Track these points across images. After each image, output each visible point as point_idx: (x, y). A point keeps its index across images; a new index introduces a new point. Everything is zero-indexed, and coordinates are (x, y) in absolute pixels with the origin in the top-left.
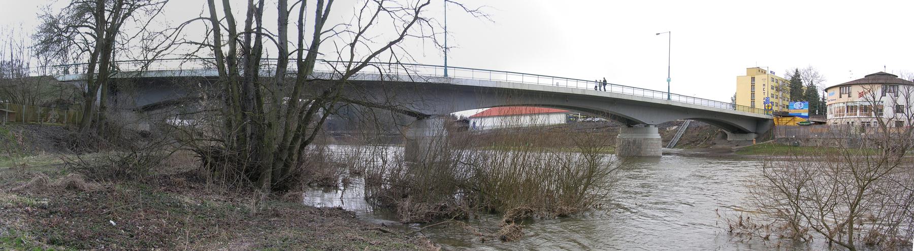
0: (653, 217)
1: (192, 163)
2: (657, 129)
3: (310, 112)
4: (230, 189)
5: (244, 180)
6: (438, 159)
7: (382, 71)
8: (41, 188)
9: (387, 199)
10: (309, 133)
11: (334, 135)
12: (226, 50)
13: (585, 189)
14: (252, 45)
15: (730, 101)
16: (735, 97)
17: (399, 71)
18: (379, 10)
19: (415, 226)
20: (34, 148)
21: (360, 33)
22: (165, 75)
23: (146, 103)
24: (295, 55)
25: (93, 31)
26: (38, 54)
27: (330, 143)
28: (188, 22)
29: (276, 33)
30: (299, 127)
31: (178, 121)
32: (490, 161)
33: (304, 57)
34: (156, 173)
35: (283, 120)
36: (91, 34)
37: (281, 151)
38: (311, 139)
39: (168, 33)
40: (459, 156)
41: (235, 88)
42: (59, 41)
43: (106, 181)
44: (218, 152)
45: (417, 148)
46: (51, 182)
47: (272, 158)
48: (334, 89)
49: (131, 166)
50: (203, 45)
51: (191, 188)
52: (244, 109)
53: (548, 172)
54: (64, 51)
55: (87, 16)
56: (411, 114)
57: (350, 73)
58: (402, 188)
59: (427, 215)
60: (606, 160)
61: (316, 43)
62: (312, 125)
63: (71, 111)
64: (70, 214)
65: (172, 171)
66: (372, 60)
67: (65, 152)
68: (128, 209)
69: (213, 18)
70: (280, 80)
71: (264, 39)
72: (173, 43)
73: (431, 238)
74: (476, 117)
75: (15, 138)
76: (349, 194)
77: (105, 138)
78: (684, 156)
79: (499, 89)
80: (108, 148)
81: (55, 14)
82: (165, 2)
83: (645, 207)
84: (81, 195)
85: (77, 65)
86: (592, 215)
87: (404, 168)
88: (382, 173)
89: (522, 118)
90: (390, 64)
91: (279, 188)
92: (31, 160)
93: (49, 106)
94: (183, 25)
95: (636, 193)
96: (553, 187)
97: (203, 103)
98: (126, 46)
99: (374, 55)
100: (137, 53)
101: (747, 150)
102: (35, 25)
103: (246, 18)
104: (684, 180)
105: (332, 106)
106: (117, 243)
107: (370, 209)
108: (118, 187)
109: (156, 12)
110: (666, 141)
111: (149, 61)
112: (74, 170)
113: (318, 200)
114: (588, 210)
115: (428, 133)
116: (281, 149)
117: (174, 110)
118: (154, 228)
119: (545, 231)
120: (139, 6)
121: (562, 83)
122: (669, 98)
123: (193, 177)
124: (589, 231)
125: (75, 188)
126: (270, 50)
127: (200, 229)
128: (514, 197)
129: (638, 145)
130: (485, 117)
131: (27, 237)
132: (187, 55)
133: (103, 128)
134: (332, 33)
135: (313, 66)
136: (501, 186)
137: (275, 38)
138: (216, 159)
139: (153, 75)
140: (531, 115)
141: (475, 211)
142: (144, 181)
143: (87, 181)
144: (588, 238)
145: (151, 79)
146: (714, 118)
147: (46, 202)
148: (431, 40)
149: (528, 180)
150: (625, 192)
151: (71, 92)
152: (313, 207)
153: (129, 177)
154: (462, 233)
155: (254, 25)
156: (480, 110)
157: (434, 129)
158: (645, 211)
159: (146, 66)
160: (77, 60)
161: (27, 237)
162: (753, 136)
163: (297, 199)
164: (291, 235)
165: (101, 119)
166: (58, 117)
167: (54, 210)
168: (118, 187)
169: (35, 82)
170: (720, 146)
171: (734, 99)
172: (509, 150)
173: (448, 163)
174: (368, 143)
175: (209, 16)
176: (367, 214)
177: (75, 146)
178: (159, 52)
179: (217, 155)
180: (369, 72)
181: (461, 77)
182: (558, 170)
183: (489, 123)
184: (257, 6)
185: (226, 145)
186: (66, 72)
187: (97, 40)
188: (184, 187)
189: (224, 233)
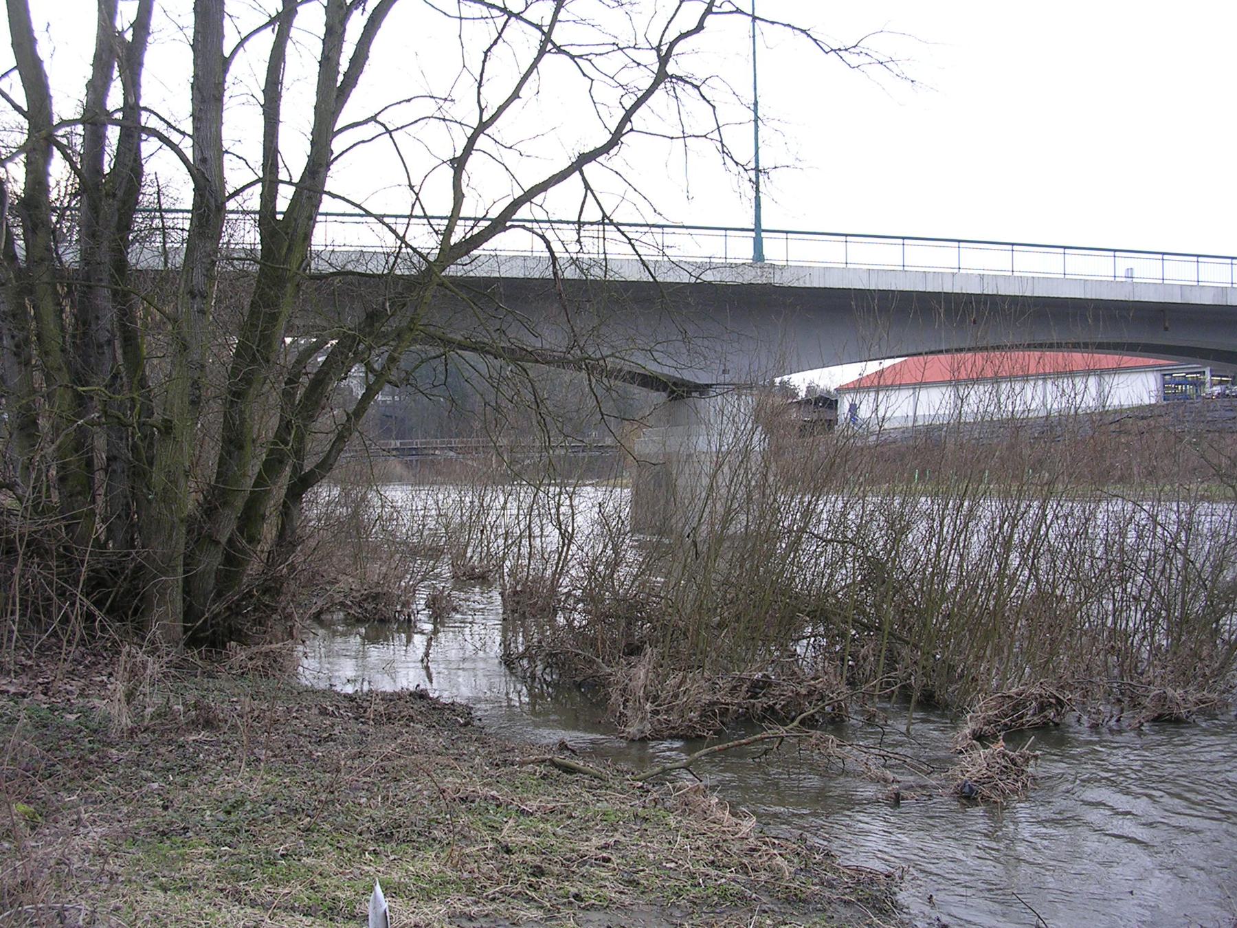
3: (320, 381)
5: (90, 617)
6: (739, 524)
7: (557, 247)
9: (578, 662)
10: (317, 447)
17: (611, 248)
18: (542, 52)
19: (669, 751)
21: (482, 127)
24: (252, 198)
27: (388, 479)
30: (285, 426)
33: (282, 204)
38: (325, 466)
40: (808, 513)
45: (672, 488)
48: (399, 304)
56: (650, 381)
57: (450, 252)
58: (624, 624)
59: (708, 712)
61: (320, 162)
62: (327, 421)
66: (523, 212)
70: (198, 279)
71: (149, 146)
73: (722, 787)
74: (857, 387)
76: (449, 645)
79: (948, 296)
87: (630, 556)
88: (559, 573)
90: (580, 224)
91: (209, 637)
99: (528, 196)
103: (89, 73)
105: (392, 360)
107: (520, 696)
113: (347, 669)
115: (704, 443)
126: (167, 176)
130: (887, 388)
134: (372, 129)
135: (308, 236)
148: (710, 148)
152: (330, 693)
154: (826, 773)
155: (115, 99)
156: (873, 367)
157: (721, 430)
163: (276, 665)
164: (255, 790)
173: (772, 537)
174: (512, 476)
176: (511, 713)
180: (513, 250)
181: (805, 259)
184: (129, 36)
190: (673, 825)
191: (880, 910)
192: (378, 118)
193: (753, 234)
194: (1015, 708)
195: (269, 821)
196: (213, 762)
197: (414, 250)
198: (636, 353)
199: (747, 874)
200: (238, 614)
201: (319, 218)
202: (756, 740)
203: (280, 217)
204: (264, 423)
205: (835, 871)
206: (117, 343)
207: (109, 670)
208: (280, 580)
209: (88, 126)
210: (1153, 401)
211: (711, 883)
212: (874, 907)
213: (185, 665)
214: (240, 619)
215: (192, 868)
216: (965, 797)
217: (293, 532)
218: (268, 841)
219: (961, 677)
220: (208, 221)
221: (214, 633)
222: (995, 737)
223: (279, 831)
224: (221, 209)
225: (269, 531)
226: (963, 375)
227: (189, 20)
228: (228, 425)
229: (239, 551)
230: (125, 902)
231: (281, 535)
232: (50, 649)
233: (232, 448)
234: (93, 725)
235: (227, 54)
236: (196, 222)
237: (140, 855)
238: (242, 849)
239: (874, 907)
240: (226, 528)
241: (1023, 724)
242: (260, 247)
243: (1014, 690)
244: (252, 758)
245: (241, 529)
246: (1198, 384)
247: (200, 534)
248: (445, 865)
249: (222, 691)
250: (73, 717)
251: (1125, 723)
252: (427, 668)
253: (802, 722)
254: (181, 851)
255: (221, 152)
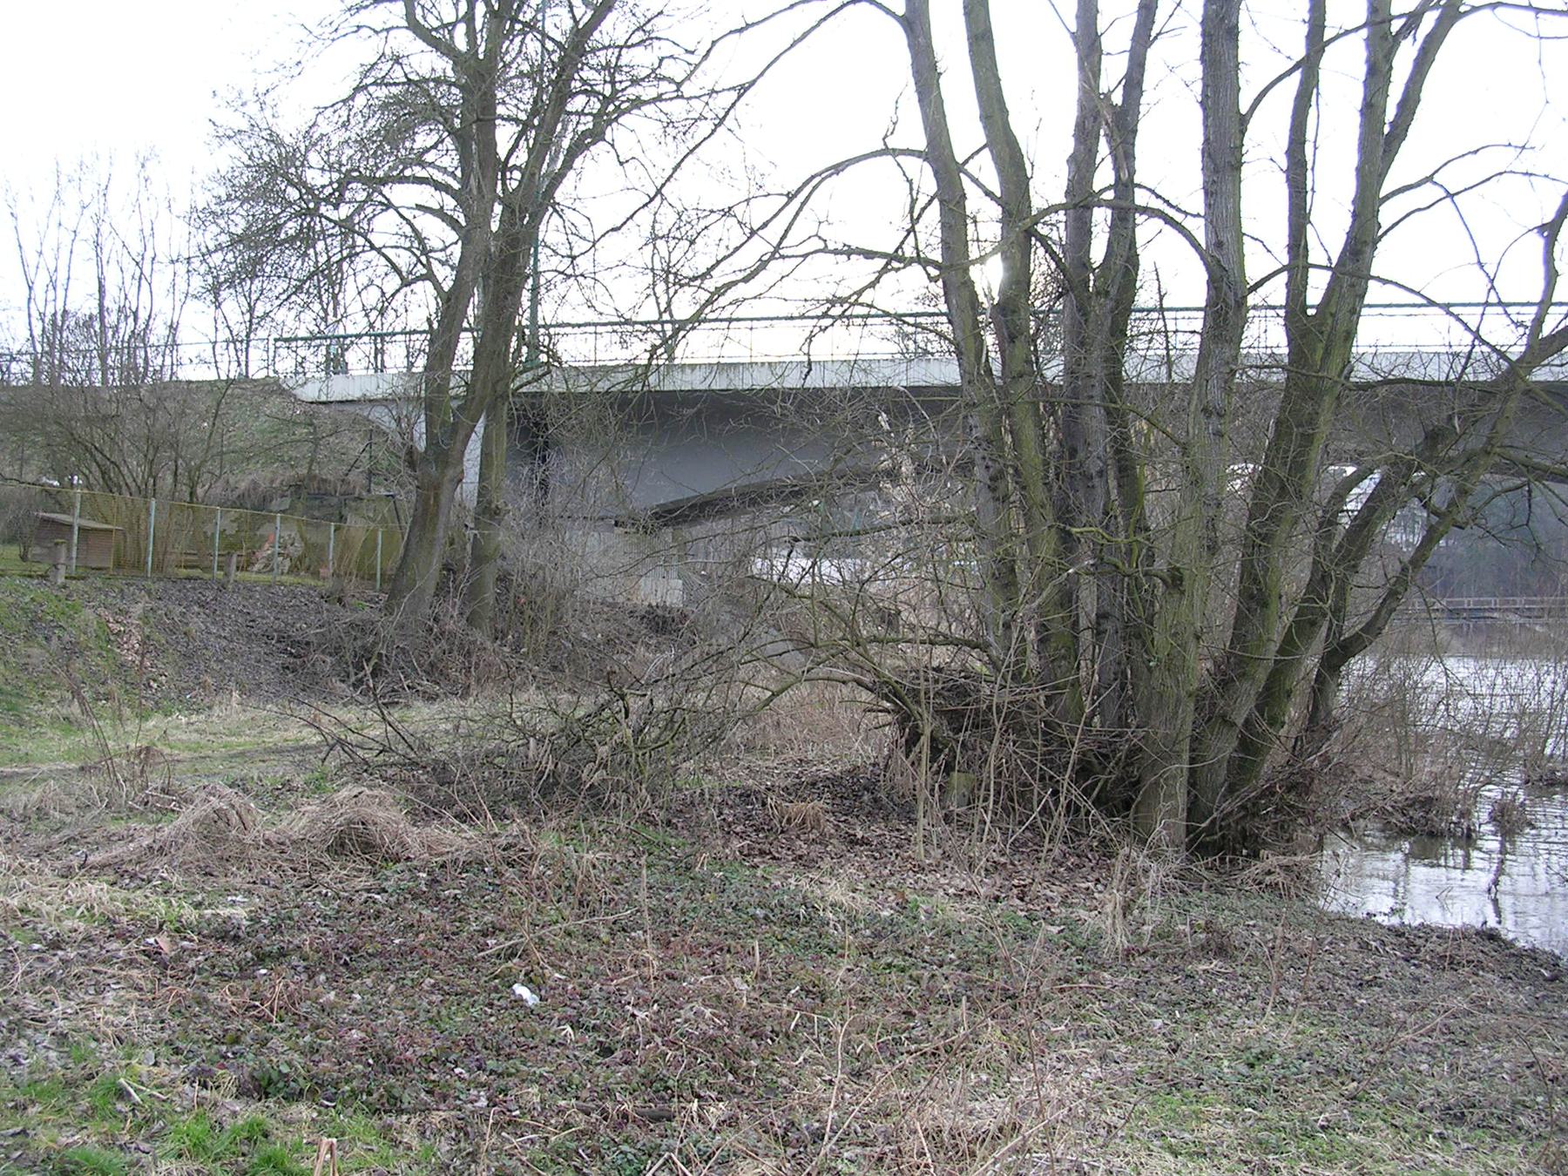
1: (856, 737)
4: (1017, 847)
5: (1073, 809)
8: (218, 848)
10: (1361, 605)
11: (1453, 613)
12: (989, 278)
14: (1098, 253)
20: (195, 679)
22: (743, 382)
23: (667, 494)
24: (1276, 292)
25: (450, 203)
26: (215, 290)
28: (837, 169)
29: (1195, 202)
30: (1320, 580)
31: (798, 565)
33: (1314, 296)
34: (709, 782)
35: (1231, 560)
36: (440, 213)
37: (1225, 684)
38: (1373, 628)
39: (756, 218)
41: (1029, 432)
42: (306, 238)
43: (502, 817)
44: (961, 692)
46: (264, 824)
47: (1188, 713)
48: (1471, 421)
49: (603, 751)
50: (895, 260)
51: (853, 841)
52: (1065, 514)
54: (328, 278)
55: (423, 139)
61: (1364, 237)
62: (1372, 573)
63: (356, 525)
64: (344, 961)
65: (769, 770)
67: (328, 696)
68: (590, 937)
69: (938, 153)
70: (1215, 395)
71: (1145, 229)
72: (776, 253)
75: (110, 638)
77: (499, 635)
80: (510, 680)
81: (290, 127)
82: (743, 89)
84: (394, 877)
85: (380, 338)
91: (1221, 843)
92: (176, 731)
93: (265, 501)
94: (814, 181)
97: (899, 494)
98: (584, 264)
100: (628, 293)
102: (197, 168)
103: (1068, 146)
106: (541, 1081)
108: (548, 843)
109: (705, 128)
111: (681, 326)
112: (362, 770)
116: (1227, 675)
117: (781, 521)
118: (698, 1016)
120: (637, 103)
123: (859, 796)
125: (368, 846)
126: (1172, 275)
127: (891, 1018)
131: (146, 1070)
132: (834, 301)
133: (489, 596)
134: (1429, 193)
135: (1350, 335)
137: (1190, 224)
138: (955, 719)
139: (694, 381)
142: (659, 816)
143: (422, 815)
145: (690, 397)
147: (238, 912)
151: (355, 446)
153: (598, 801)
155: (1104, 176)
159: (669, 343)
160: (381, 321)
161: (146, 1070)
163: (1303, 882)
165: (479, 558)
166: (297, 549)
167: (273, 943)
168: (548, 843)
169: (205, 403)
175: (921, 143)
177: (370, 669)
178: (720, 291)
179: (960, 707)
184: (1117, 99)
185: (994, 664)
186: (336, 365)
187: (466, 236)
188: (822, 841)
189: (992, 1033)
192: (1436, 178)
195: (1304, 1082)
196: (1229, 1000)
197: (1494, 348)
200: (1254, 815)
201: (1364, 311)
203: (1311, 312)
204: (1292, 576)
206: (1111, 473)
207: (1096, 875)
208: (1309, 775)
209: (1071, 212)
213: (1187, 874)
214: (1257, 822)
215: (1208, 1131)
217: (1329, 714)
218: (1302, 1107)
220: (1225, 320)
221: (1223, 837)
223: (1317, 1095)
224: (1241, 303)
225: (1294, 712)
227: (1197, 70)
228: (1248, 573)
229: (1258, 735)
230: (1128, 1163)
231: (1313, 718)
232: (1025, 844)
233: (1254, 606)
234: (1081, 942)
235: (1244, 109)
236: (1210, 322)
237: (1143, 1106)
238: (1270, 1113)
240: (1243, 708)
242: (1286, 351)
244: (1278, 999)
245: (1260, 708)
247: (1212, 712)
248: (1537, 1164)
249: (1234, 911)
250: (1055, 930)
252: (1495, 901)
254: (1194, 1107)
255: (1239, 235)
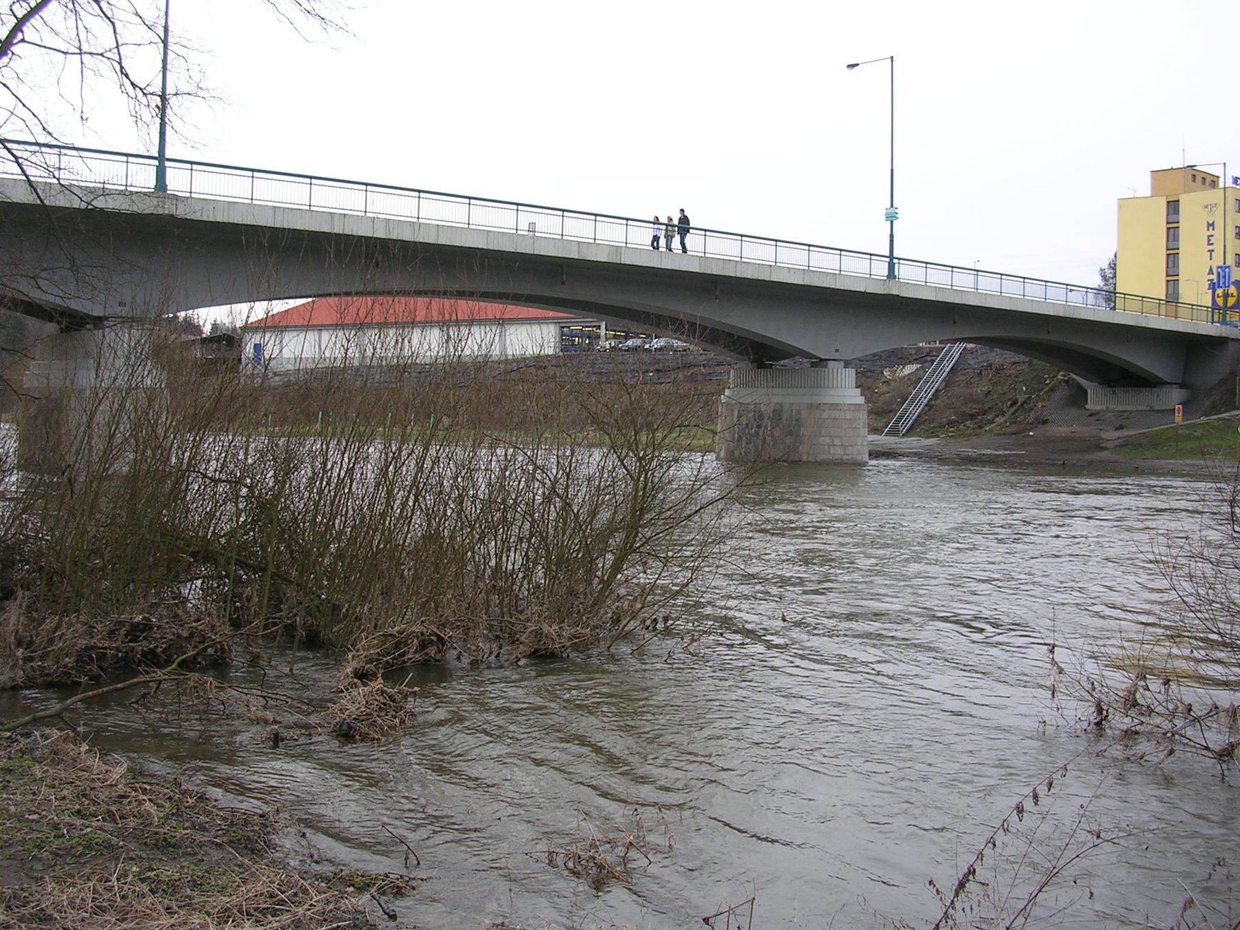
0: (842, 663)
2: (851, 373)
6: (122, 467)
13: (617, 568)
15: (1097, 281)
16: (1113, 266)
32: (305, 472)
53: (498, 511)
59: (83, 657)
60: (686, 470)
78: (942, 460)
83: (812, 630)
86: (640, 652)
89: (416, 335)
95: (784, 582)
96: (514, 560)
101: (1154, 443)
104: (944, 540)
110: (882, 413)
114: (627, 636)
119: (484, 707)
121: (548, 226)
122: (891, 274)
124: (629, 706)
128: (386, 593)
129: (788, 425)
136: (340, 555)
140: (444, 324)
141: (250, 638)
144: (627, 729)
146: (1042, 336)
149: (432, 537)
150: (749, 578)
154: (204, 714)
156: (279, 306)
157: (116, 363)
158: (815, 642)
162: (1174, 397)
170: (1061, 430)
171: (1110, 274)
172: (370, 440)
181: (204, 189)
182: (530, 504)
183: (296, 350)
190: (39, 775)
191: (252, 850)
193: (156, 162)
194: (397, 646)
198: (20, 279)
199: (115, 821)
202: (138, 683)
205: (208, 813)
210: (551, 352)
211: (76, 833)
212: (246, 847)
216: (343, 736)
219: (346, 616)
222: (375, 675)
226: (349, 320)
239: (246, 847)
241: (404, 662)
243: (397, 628)
246: (595, 337)
251: (503, 658)
253: (181, 664)
